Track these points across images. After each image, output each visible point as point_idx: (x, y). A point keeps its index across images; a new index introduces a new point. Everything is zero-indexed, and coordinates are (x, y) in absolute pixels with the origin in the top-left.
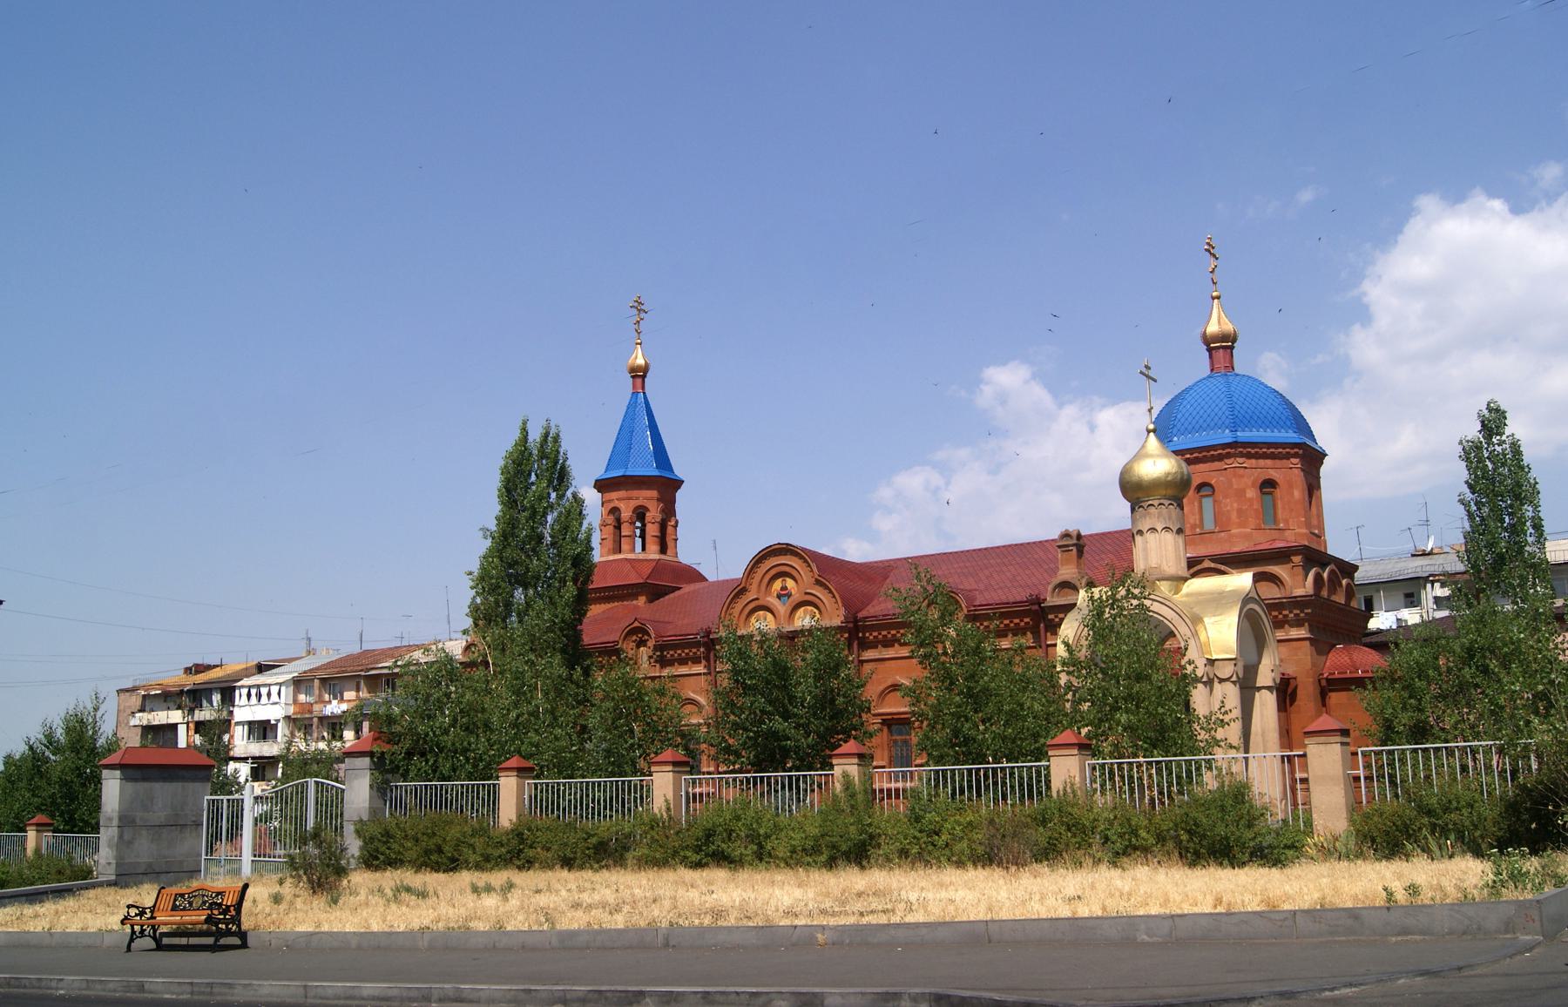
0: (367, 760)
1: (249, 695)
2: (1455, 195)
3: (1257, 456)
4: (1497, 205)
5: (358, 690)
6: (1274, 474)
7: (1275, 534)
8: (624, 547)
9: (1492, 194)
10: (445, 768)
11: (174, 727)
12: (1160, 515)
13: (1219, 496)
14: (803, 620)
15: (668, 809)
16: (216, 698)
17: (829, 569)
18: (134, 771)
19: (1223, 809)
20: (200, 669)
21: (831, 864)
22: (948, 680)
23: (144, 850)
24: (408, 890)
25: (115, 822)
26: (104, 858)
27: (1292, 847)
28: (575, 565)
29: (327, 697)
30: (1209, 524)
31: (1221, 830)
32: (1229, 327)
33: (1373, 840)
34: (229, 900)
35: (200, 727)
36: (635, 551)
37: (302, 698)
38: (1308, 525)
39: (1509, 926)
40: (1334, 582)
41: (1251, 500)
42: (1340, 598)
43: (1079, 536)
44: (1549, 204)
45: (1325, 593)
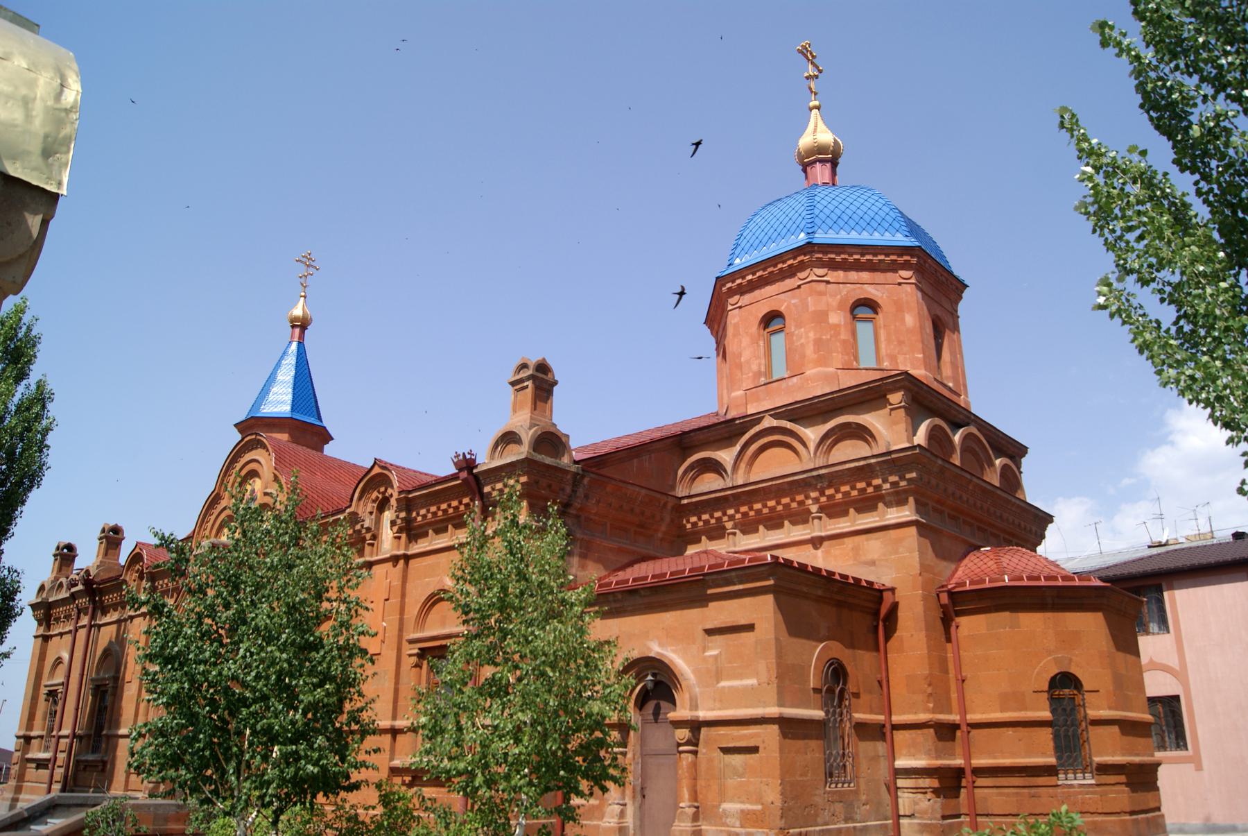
6: (872, 292)
30: (779, 371)
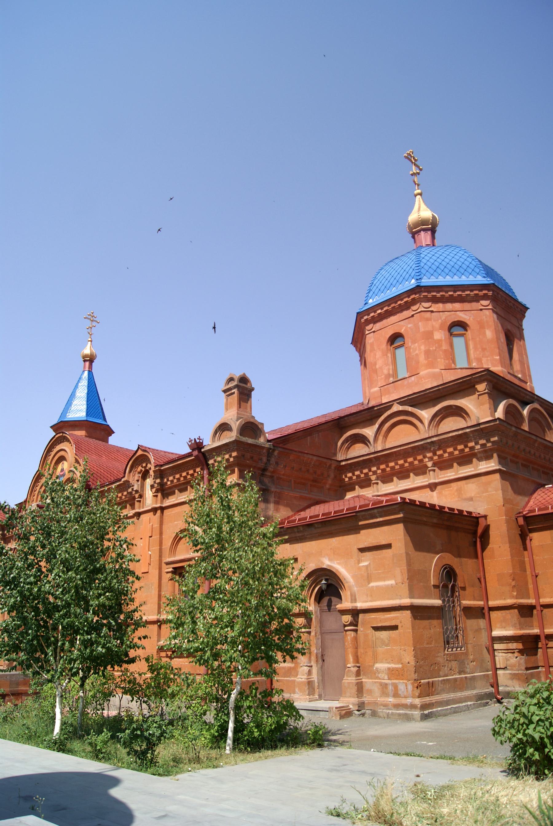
6: (463, 316)
13: (408, 341)
41: (439, 341)
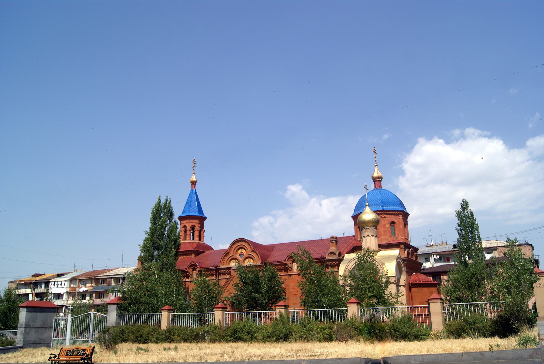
0: (115, 306)
1: (54, 284)
2: (429, 138)
3: (389, 214)
4: (441, 141)
5: (91, 283)
6: (395, 220)
7: (395, 238)
8: (187, 238)
9: (440, 138)
10: (142, 309)
11: (27, 295)
12: (370, 231)
14: (248, 263)
15: (220, 323)
16: (43, 286)
17: (256, 247)
18: (31, 309)
19: (404, 323)
20: (37, 275)
21: (277, 341)
22: (311, 281)
23: (33, 336)
24: (142, 349)
25: (24, 326)
26: (19, 338)
27: (425, 335)
28: (175, 243)
29: (81, 285)
31: (405, 329)
32: (380, 175)
33: (452, 333)
34: (88, 352)
35: (37, 295)
36: (190, 240)
37: (72, 286)
38: (405, 236)
39: (531, 357)
40: (412, 254)
42: (414, 259)
43: (336, 238)
44: (457, 142)
45: (410, 257)
